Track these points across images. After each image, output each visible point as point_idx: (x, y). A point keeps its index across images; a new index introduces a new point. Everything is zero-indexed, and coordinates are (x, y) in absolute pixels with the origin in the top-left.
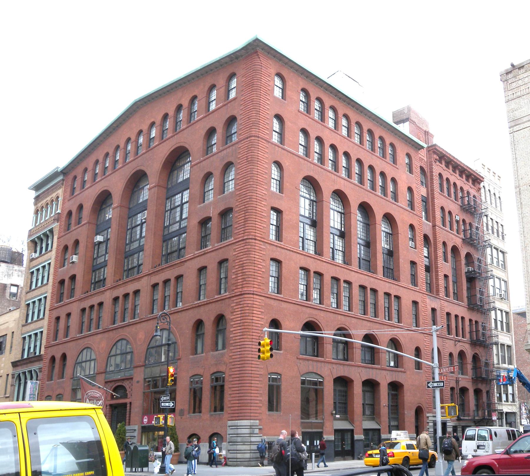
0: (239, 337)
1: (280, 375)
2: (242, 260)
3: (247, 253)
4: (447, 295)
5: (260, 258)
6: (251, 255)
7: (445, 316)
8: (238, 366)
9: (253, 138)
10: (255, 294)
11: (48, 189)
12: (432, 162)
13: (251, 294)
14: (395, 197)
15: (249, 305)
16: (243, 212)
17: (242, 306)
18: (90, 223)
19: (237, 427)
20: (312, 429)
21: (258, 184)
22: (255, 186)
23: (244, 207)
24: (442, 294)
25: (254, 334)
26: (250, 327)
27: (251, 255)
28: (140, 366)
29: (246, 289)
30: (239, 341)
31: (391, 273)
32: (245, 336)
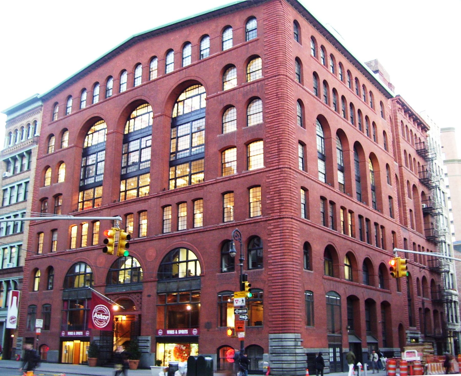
0: (279, 257)
1: (312, 292)
2: (278, 186)
3: (284, 180)
4: (413, 228)
5: (295, 185)
6: (287, 183)
7: (412, 245)
8: (280, 284)
9: (282, 76)
10: (294, 219)
11: (23, 114)
12: (395, 110)
13: (290, 218)
14: (376, 139)
15: (289, 228)
16: (276, 143)
17: (281, 229)
18: (77, 146)
19: (281, 340)
20: (334, 342)
21: (289, 118)
22: (287, 120)
23: (276, 138)
24: (409, 226)
25: (294, 255)
26: (291, 248)
27: (287, 183)
28: (151, 281)
29: (284, 213)
30: (280, 260)
31: (378, 206)
32: (286, 257)
